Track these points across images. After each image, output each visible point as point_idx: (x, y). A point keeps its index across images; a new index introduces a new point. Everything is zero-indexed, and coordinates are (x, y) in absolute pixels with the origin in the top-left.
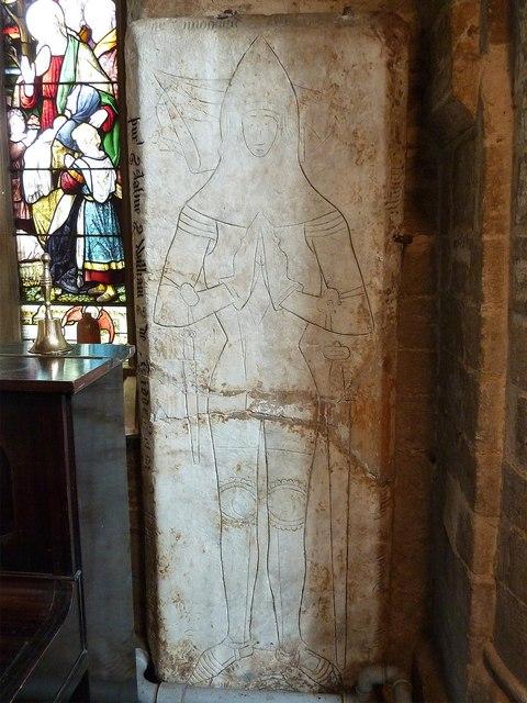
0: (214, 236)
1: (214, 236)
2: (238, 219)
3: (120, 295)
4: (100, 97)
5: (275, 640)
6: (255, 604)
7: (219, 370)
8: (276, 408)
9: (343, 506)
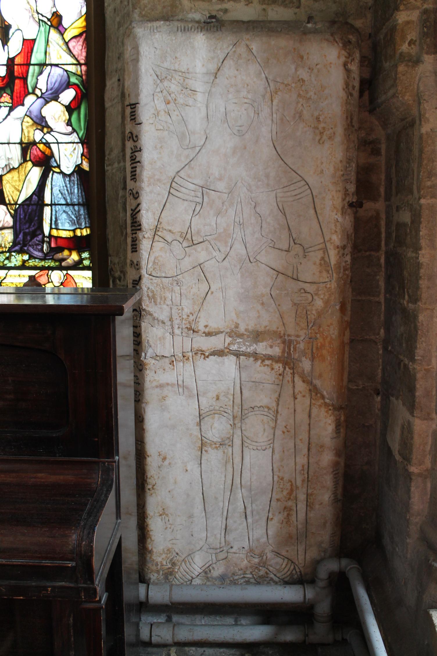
0: (199, 200)
1: (199, 200)
2: (221, 186)
3: (84, 259)
4: (69, 77)
5: (246, 545)
6: (229, 515)
7: (202, 314)
8: (250, 346)
9: (305, 427)
